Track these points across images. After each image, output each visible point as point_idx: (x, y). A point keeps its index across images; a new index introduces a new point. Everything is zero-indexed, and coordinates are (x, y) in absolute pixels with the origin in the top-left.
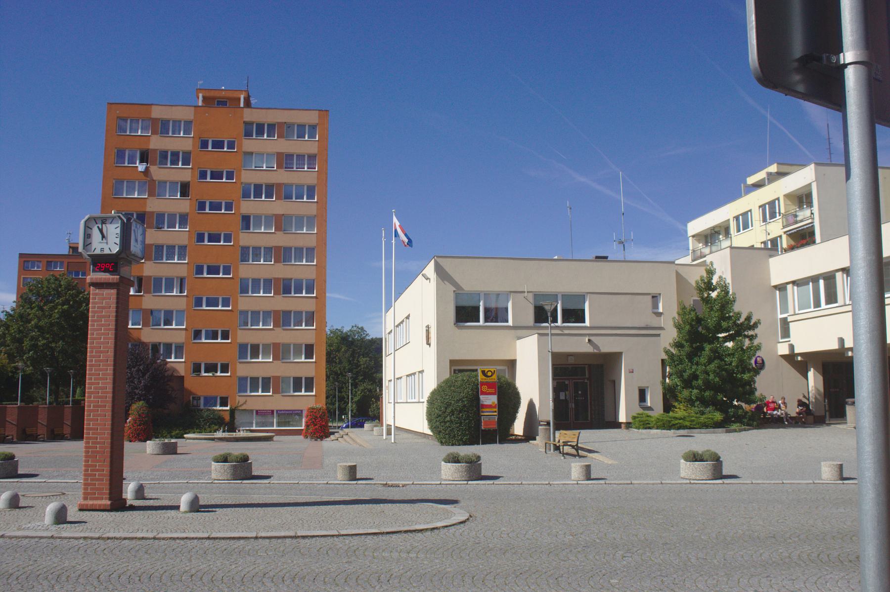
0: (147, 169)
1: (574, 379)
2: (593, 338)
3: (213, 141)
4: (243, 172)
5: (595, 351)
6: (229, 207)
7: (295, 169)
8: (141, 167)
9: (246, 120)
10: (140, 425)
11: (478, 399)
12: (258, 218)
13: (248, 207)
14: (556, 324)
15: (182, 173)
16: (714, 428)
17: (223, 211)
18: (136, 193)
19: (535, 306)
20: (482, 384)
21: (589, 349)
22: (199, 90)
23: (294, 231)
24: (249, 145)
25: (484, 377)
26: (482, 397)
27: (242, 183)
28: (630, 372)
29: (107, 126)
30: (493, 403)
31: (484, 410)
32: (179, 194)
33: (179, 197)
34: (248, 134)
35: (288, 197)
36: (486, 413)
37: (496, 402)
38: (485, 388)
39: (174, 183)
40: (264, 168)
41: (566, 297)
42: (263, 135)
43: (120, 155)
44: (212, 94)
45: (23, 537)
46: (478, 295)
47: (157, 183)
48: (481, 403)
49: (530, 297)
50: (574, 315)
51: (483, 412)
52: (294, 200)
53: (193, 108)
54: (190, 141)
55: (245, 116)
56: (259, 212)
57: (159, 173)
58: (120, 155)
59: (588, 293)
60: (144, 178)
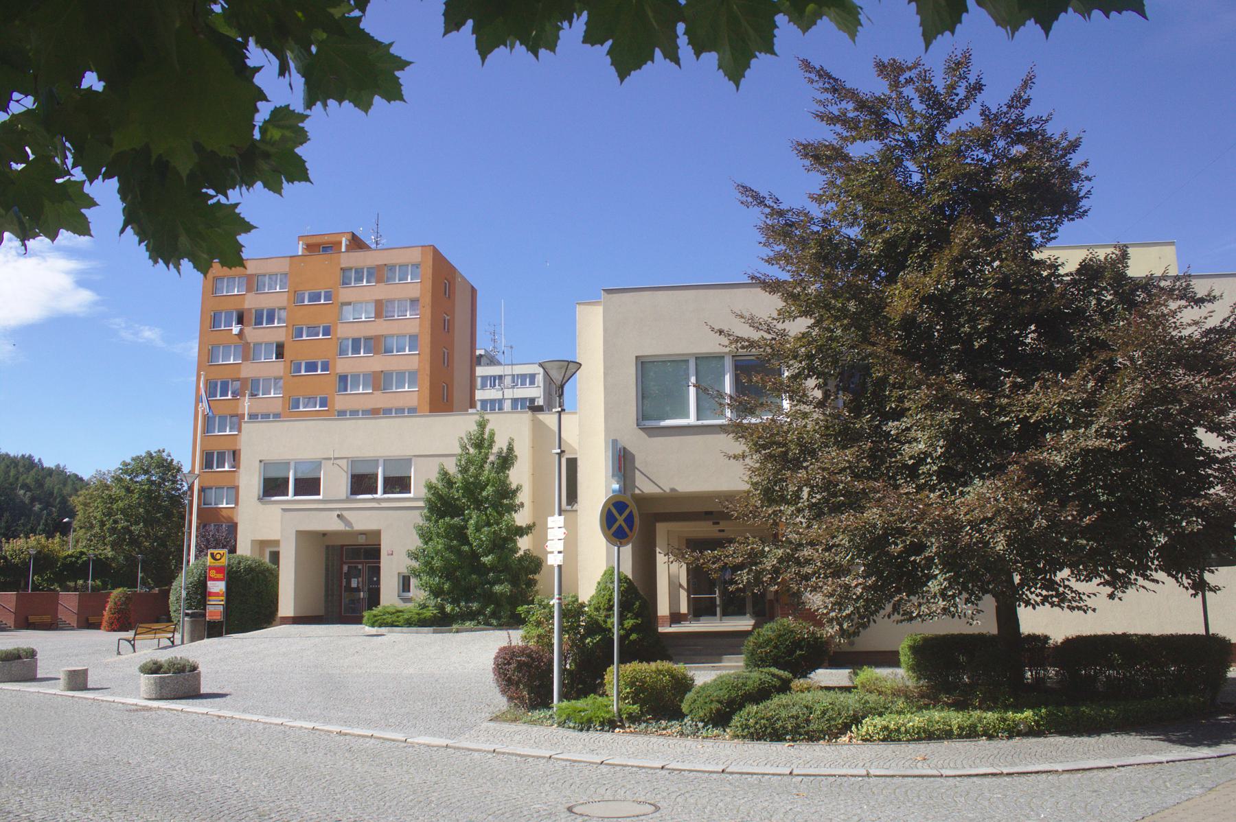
0: (241, 331)
1: (369, 563)
2: (345, 513)
3: (309, 294)
4: (340, 325)
5: (347, 529)
6: (326, 367)
7: (396, 317)
8: (236, 329)
9: (343, 266)
10: (115, 613)
11: (205, 586)
12: (356, 377)
13: (344, 365)
14: (375, 496)
15: (276, 332)
16: (419, 626)
17: (319, 372)
18: (232, 358)
19: (264, 479)
20: (211, 568)
21: (338, 526)
22: (300, 238)
23: (394, 390)
24: (345, 294)
25: (213, 561)
26: (209, 583)
27: (338, 339)
28: (388, 555)
29: (203, 288)
30: (221, 590)
31: (210, 598)
32: (274, 356)
33: (274, 359)
34: (345, 283)
35: (388, 351)
36: (212, 601)
37: (224, 590)
38: (213, 573)
39: (268, 344)
40: (363, 319)
41: (388, 462)
42: (362, 281)
43: (215, 321)
44: (314, 240)
45: (851, 776)
46: (375, 462)
47: (252, 345)
48: (208, 590)
49: (343, 463)
50: (309, 486)
51: (209, 601)
52: (395, 353)
53: (420, 248)
54: (285, 296)
55: (342, 261)
56: (356, 370)
57: (254, 334)
58: (215, 321)
59: (415, 456)
60: (238, 340)
